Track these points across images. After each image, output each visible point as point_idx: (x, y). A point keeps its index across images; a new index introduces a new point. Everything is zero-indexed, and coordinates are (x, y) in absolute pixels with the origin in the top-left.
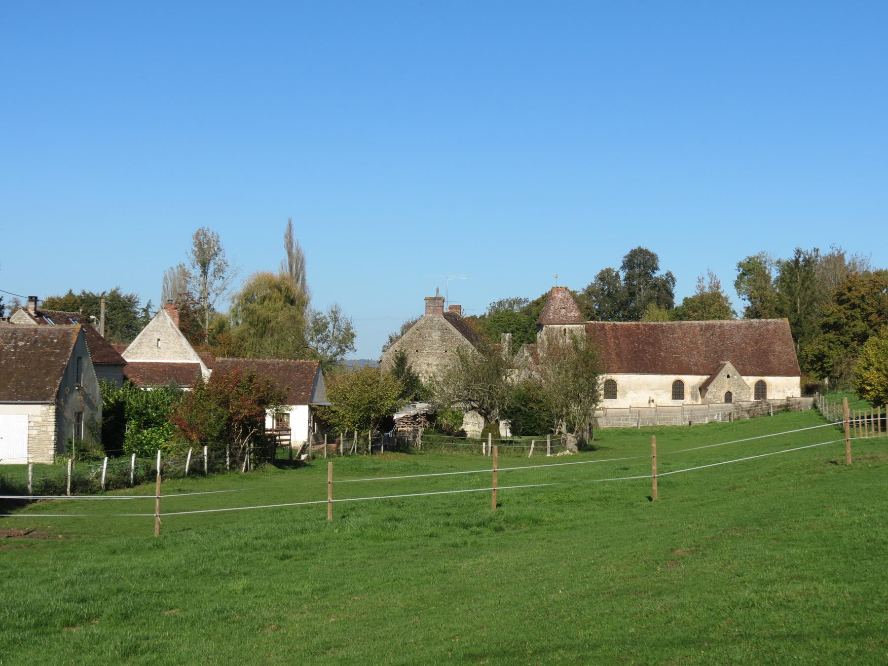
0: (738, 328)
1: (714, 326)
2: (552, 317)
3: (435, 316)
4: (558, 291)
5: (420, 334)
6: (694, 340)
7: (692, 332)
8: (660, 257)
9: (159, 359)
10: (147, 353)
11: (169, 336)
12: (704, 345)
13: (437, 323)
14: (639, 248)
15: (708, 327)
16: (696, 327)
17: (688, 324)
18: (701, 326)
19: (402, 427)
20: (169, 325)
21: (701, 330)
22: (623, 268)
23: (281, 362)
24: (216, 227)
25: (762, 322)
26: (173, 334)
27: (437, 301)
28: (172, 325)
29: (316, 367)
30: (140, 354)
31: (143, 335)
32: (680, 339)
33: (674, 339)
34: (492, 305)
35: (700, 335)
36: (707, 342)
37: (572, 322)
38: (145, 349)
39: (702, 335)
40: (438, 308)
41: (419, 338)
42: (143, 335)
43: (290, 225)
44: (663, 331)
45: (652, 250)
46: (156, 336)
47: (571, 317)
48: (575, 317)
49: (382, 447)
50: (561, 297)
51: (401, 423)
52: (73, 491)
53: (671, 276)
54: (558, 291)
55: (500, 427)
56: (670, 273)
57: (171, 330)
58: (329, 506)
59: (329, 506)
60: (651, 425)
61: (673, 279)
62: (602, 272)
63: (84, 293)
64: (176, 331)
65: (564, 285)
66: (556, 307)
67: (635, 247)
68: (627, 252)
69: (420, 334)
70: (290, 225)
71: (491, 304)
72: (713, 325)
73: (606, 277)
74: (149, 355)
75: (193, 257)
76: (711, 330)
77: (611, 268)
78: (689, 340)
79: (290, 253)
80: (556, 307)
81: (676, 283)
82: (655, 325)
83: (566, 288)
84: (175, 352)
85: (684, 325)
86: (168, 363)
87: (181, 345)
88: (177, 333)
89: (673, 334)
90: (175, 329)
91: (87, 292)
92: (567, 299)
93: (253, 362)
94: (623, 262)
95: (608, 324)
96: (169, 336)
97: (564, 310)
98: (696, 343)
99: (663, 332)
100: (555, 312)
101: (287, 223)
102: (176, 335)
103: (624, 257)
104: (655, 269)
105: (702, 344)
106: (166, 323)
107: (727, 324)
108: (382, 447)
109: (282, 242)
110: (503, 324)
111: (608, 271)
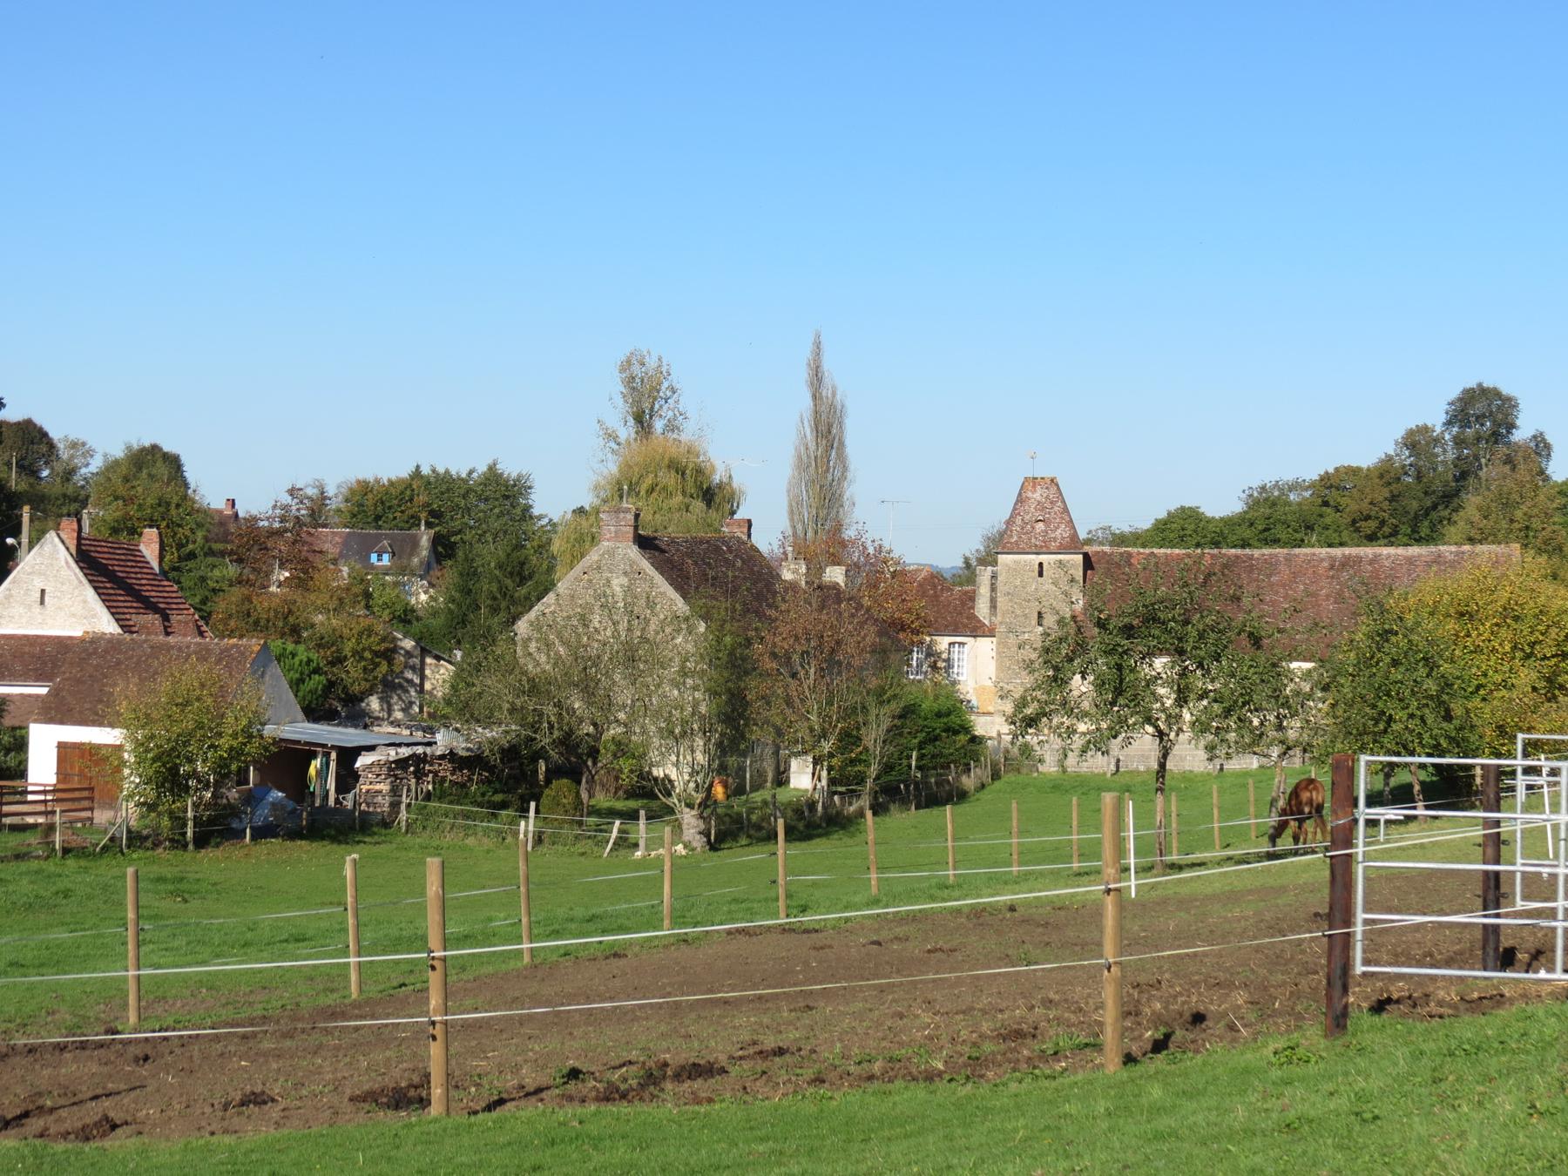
0: (1411, 564)
1: (1359, 560)
2: (1015, 538)
3: (618, 544)
4: (1034, 486)
5: (590, 581)
6: (1313, 588)
7: (1311, 571)
8: (1523, 406)
9: (42, 628)
10: (21, 616)
11: (63, 584)
12: (1332, 600)
13: (622, 559)
14: (1480, 385)
15: (1346, 563)
16: (1322, 560)
17: (1306, 555)
18: (1332, 559)
19: (371, 783)
20: (63, 563)
21: (1332, 567)
22: (1449, 423)
23: (196, 644)
24: (659, 348)
25: (1463, 553)
26: (69, 581)
27: (622, 515)
28: (67, 563)
29: (254, 655)
30: (8, 619)
31: (14, 582)
32: (1284, 586)
33: (1272, 585)
34: (1247, 492)
35: (1328, 577)
36: (1340, 594)
37: (1034, 549)
38: (17, 610)
39: (1332, 577)
40: (623, 529)
41: (587, 588)
42: (14, 582)
43: (818, 346)
44: (1251, 569)
45: (1506, 390)
46: (39, 584)
47: (1055, 539)
48: (1063, 538)
49: (248, 830)
50: (1039, 498)
51: (370, 775)
52: (1098, 829)
53: (1544, 440)
54: (1034, 486)
55: (792, 770)
56: (1541, 434)
57: (65, 573)
58: (1518, 876)
59: (1518, 876)
60: (1142, 768)
61: (1548, 447)
62: (1411, 433)
63: (434, 471)
64: (75, 574)
65: (1048, 474)
66: (1027, 518)
67: (1472, 384)
68: (1455, 392)
69: (590, 581)
70: (818, 346)
71: (1244, 491)
72: (1356, 556)
73: (1417, 441)
74: (24, 620)
75: (620, 401)
76: (1352, 567)
77: (1430, 425)
78: (1302, 587)
79: (816, 397)
80: (1027, 518)
81: (1552, 454)
82: (1237, 557)
83: (1052, 480)
84: (74, 615)
85: (1297, 556)
86: (58, 637)
87: (85, 602)
88: (78, 578)
89: (1270, 575)
90: (72, 570)
91: (441, 470)
92: (1051, 503)
93: (145, 641)
94: (1447, 413)
95: (1139, 553)
96: (63, 584)
97: (1041, 524)
98: (1314, 595)
99: (1251, 572)
100: (1022, 529)
101: (811, 339)
102: (76, 582)
103: (1449, 404)
104: (1511, 426)
105: (1328, 596)
106: (56, 559)
107: (1389, 556)
108: (248, 830)
109: (803, 375)
110: (1172, 535)
111: (1425, 430)
